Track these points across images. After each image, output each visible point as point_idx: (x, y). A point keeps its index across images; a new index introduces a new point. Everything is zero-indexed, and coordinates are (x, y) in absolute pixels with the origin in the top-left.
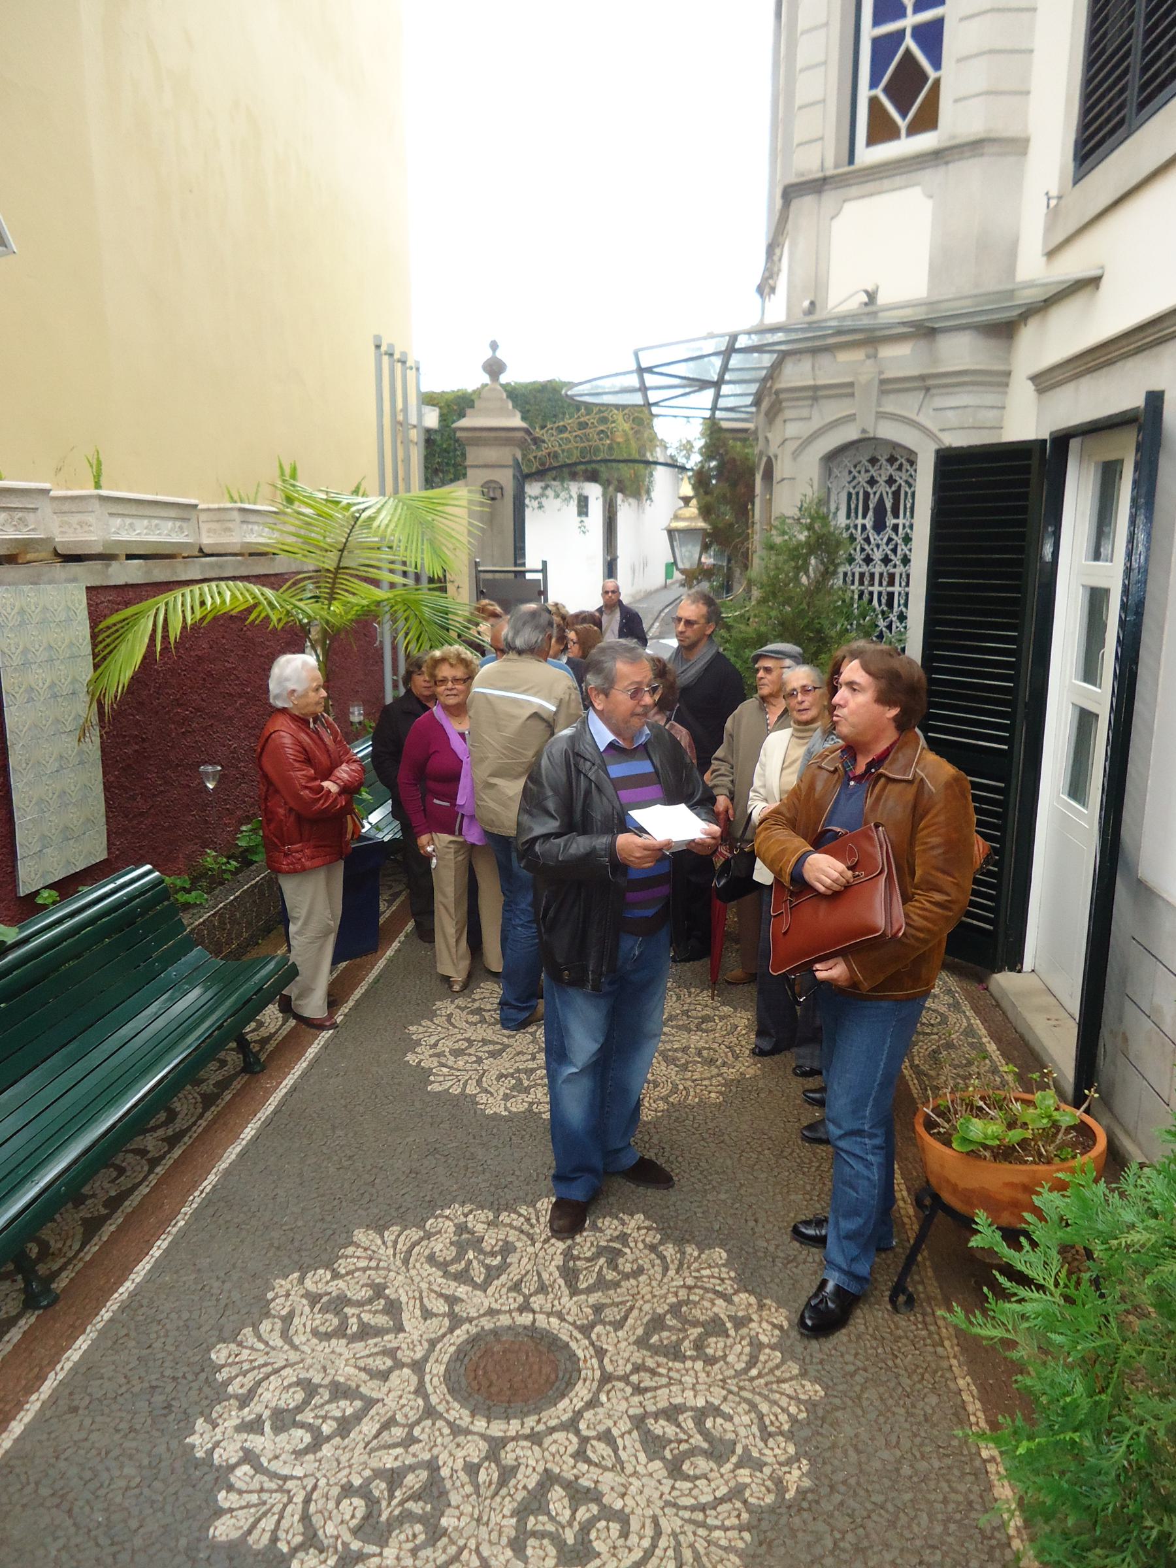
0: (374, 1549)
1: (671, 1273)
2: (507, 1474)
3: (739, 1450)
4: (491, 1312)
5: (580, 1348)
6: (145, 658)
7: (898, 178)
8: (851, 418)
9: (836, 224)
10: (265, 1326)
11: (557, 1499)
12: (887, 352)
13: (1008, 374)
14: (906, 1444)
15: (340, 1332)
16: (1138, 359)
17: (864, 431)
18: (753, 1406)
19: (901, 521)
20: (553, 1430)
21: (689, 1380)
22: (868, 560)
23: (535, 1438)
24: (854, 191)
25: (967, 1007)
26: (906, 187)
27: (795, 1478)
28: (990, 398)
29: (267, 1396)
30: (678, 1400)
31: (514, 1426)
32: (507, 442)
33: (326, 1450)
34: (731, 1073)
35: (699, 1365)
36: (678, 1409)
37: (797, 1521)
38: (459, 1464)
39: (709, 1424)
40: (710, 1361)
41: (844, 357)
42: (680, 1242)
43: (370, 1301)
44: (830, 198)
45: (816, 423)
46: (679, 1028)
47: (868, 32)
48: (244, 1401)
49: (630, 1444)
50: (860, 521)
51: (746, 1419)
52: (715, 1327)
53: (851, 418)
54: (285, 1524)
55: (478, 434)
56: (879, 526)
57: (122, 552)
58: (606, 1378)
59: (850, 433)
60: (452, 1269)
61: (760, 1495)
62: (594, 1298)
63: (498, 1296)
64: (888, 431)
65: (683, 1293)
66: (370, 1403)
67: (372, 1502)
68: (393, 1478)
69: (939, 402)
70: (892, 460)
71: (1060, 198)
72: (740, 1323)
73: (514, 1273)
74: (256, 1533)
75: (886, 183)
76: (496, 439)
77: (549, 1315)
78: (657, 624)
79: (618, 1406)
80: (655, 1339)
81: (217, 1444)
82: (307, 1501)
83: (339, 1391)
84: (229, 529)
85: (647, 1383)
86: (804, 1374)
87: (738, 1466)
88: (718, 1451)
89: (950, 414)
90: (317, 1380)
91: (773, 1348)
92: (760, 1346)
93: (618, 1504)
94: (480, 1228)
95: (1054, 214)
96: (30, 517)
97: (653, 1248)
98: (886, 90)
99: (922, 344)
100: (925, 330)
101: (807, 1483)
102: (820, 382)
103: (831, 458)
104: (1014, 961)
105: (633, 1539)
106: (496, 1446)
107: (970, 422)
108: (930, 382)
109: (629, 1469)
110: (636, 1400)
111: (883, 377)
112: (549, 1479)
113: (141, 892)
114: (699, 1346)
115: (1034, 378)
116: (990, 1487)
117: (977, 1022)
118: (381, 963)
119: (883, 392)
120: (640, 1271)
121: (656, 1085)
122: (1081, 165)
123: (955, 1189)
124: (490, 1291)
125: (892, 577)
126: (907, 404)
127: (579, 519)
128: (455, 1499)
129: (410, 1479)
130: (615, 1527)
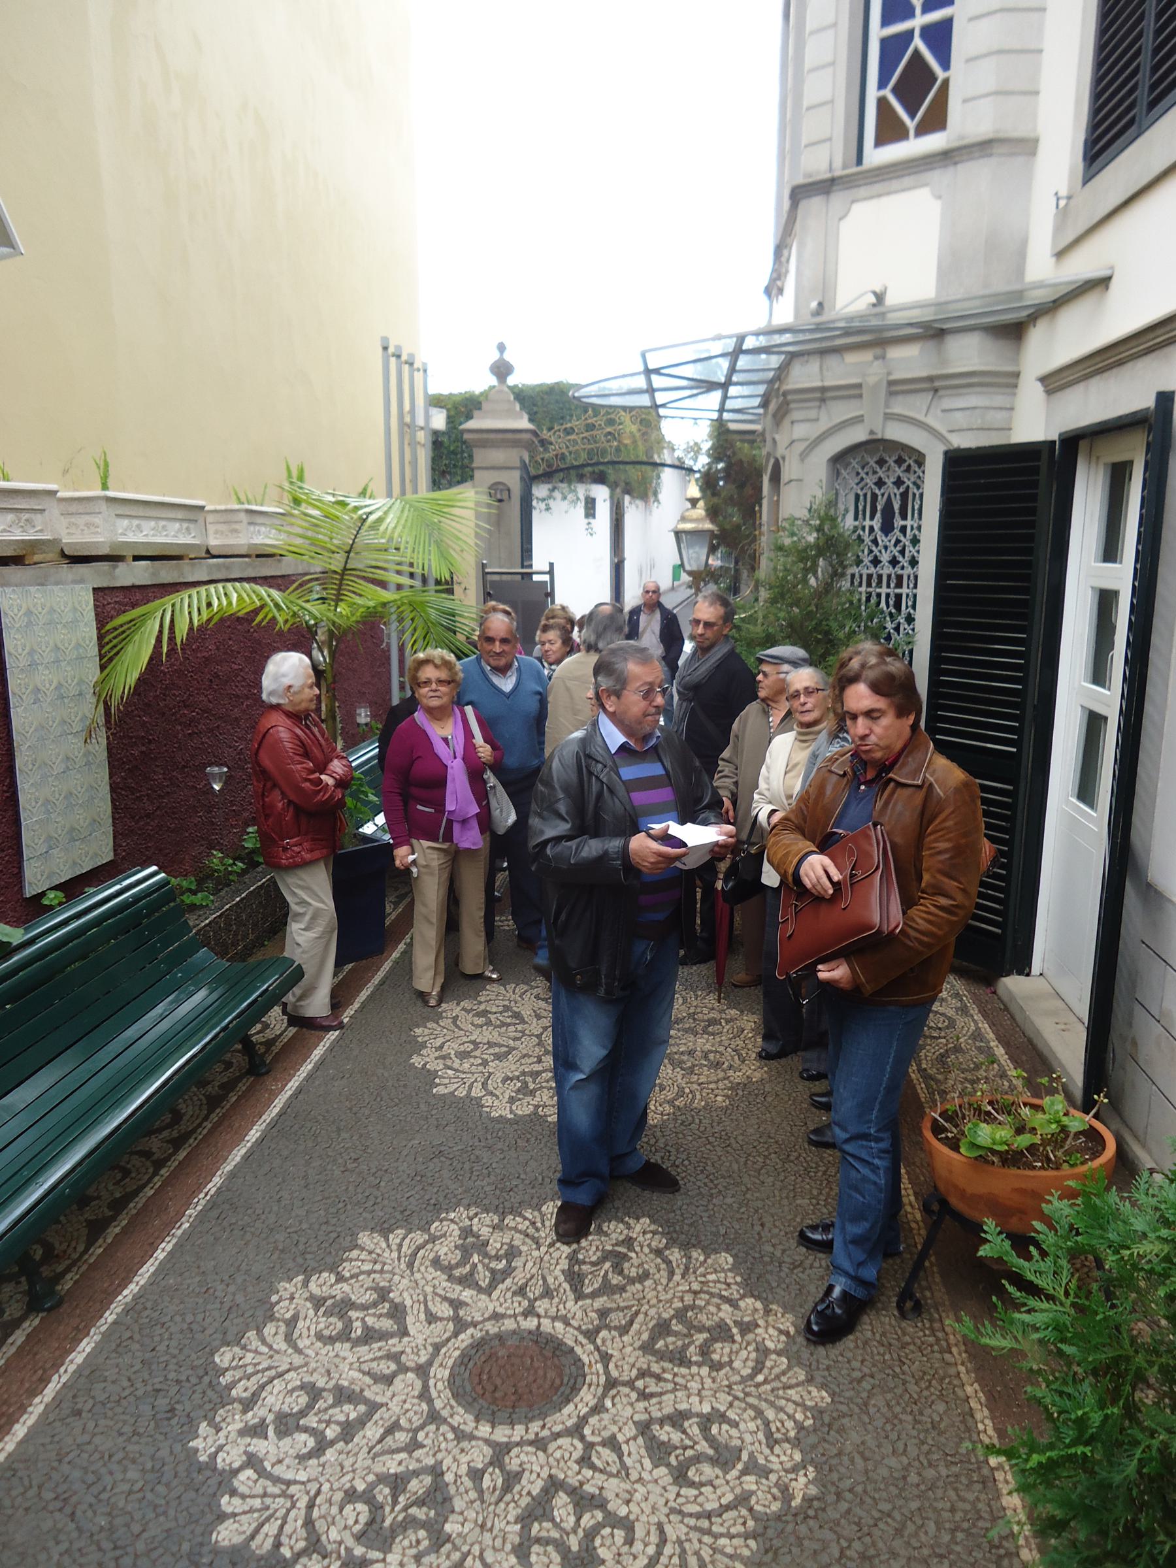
1: (677, 1278)
2: (512, 1479)
3: (745, 1456)
4: (496, 1316)
5: (585, 1353)
6: (151, 659)
8: (859, 420)
9: (843, 224)
10: (269, 1330)
11: (562, 1506)
12: (896, 353)
14: (913, 1451)
17: (872, 432)
18: (759, 1413)
19: (909, 523)
20: (558, 1435)
21: (694, 1385)
22: (876, 562)
23: (540, 1444)
24: (862, 191)
25: (974, 1010)
26: (914, 188)
27: (801, 1485)
28: (999, 400)
29: (270, 1400)
30: (683, 1406)
32: (516, 444)
33: (330, 1455)
34: (737, 1077)
35: (705, 1371)
36: (684, 1415)
37: (803, 1529)
38: (464, 1469)
39: (714, 1430)
40: (716, 1367)
41: (851, 358)
42: (686, 1247)
43: (375, 1305)
44: (838, 199)
45: (824, 424)
46: (686, 1031)
47: (877, 32)
48: (248, 1405)
49: (635, 1451)
50: (867, 523)
51: (752, 1426)
52: (721, 1332)
53: (859, 420)
54: (288, 1529)
55: (485, 436)
56: (887, 528)
58: (611, 1383)
59: (859, 435)
60: (457, 1273)
61: (766, 1503)
62: (600, 1302)
63: (502, 1301)
64: (896, 433)
65: (688, 1298)
66: (374, 1407)
67: (376, 1508)
68: (397, 1483)
70: (899, 461)
71: (1069, 198)
72: (747, 1328)
73: (519, 1277)
74: (259, 1538)
76: (503, 440)
79: (624, 1412)
80: (660, 1344)
81: (220, 1448)
82: (311, 1506)
83: (343, 1395)
84: (236, 531)
85: (653, 1388)
86: (810, 1380)
87: (744, 1472)
88: (724, 1457)
89: (958, 415)
90: (321, 1383)
91: (779, 1353)
92: (767, 1352)
93: (623, 1511)
94: (485, 1231)
95: (1063, 215)
97: (658, 1252)
98: (895, 91)
99: (930, 345)
100: (933, 332)
101: (813, 1491)
102: (827, 383)
103: (839, 460)
104: (1023, 965)
105: (638, 1546)
106: (500, 1451)
107: (979, 423)
108: (937, 384)
109: (634, 1476)
110: (641, 1405)
111: (892, 378)
112: (553, 1485)
114: (705, 1351)
115: (1043, 380)
117: (985, 1026)
119: (892, 394)
120: (646, 1275)
123: (962, 1194)
124: (495, 1295)
125: (900, 578)
126: (915, 406)
128: (458, 1504)
129: (414, 1485)
130: (620, 1534)
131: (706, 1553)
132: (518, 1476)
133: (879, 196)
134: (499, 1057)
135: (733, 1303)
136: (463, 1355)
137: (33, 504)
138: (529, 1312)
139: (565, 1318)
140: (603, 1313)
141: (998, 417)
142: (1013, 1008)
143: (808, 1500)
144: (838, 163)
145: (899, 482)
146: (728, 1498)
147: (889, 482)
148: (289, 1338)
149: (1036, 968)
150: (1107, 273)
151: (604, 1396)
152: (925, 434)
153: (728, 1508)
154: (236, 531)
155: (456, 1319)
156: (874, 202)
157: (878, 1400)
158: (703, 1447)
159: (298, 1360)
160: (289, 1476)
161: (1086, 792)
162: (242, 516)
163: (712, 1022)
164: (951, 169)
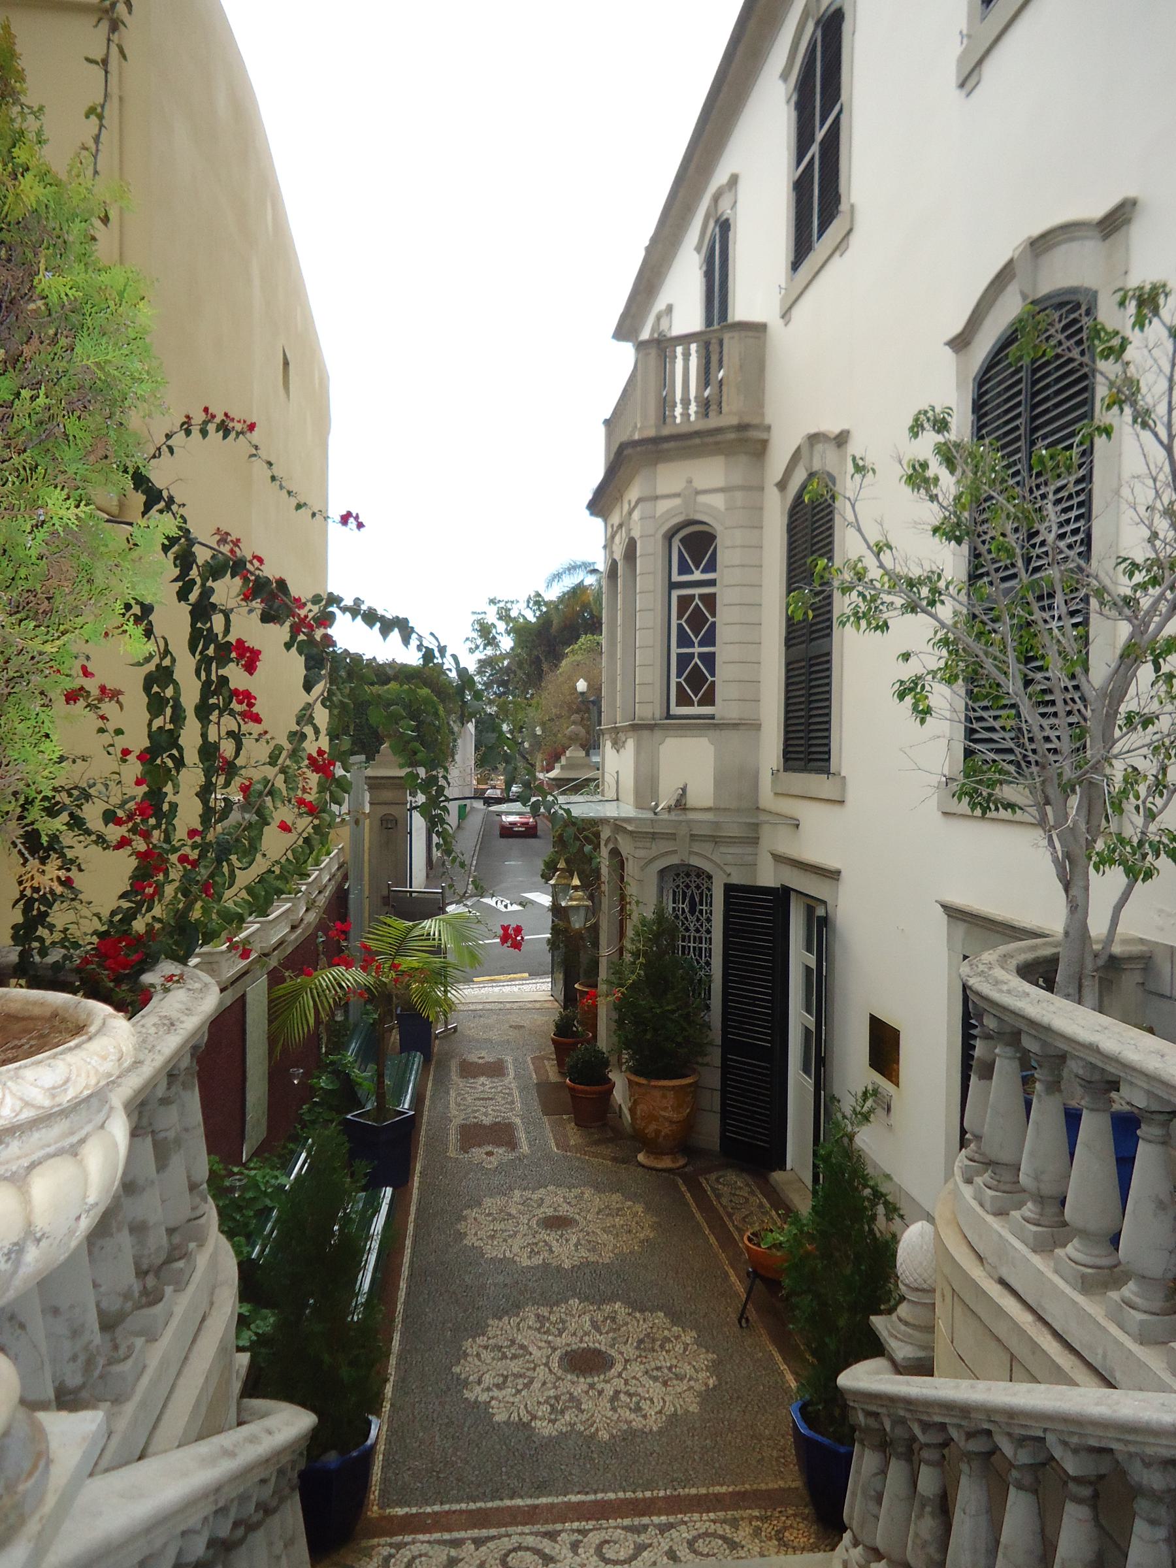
5: (612, 1352)
8: (675, 852)
19: (704, 908)
22: (687, 930)
25: (758, 1192)
27: (711, 1382)
28: (749, 850)
42: (642, 1311)
44: (658, 734)
45: (654, 852)
47: (675, 651)
52: (667, 1340)
53: (675, 852)
56: (692, 912)
58: (627, 1361)
59: (674, 860)
61: (698, 1387)
62: (611, 1335)
63: (565, 1338)
64: (695, 861)
68: (557, 1398)
69: (723, 849)
72: (678, 1337)
75: (688, 732)
98: (685, 680)
103: (662, 872)
104: (782, 1165)
112: (617, 1393)
125: (701, 938)
126: (706, 848)
135: (669, 1330)
138: (581, 1341)
139: (600, 1342)
143: (715, 1386)
144: (657, 715)
145: (698, 887)
147: (693, 885)
149: (788, 1167)
163: (619, 1209)
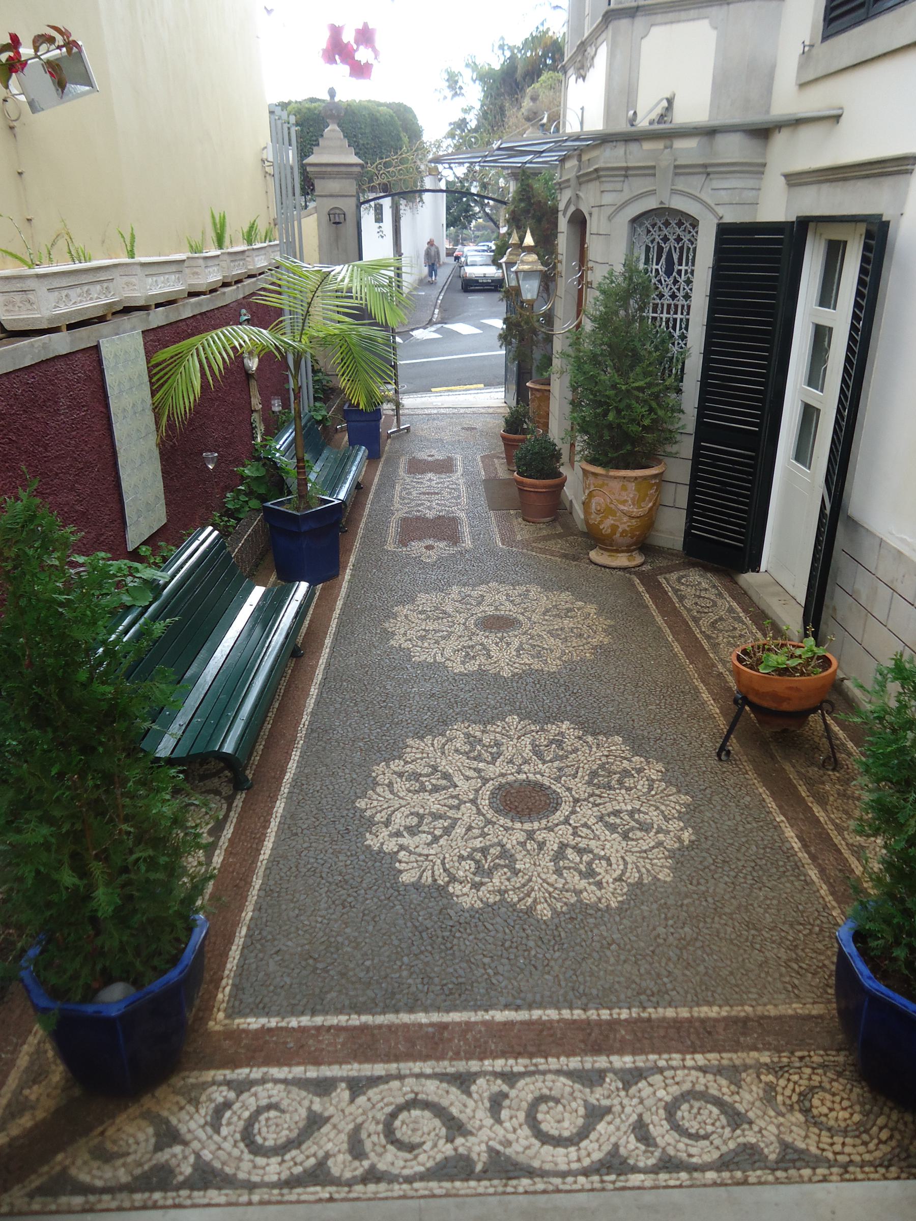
0: (487, 880)
1: (594, 749)
2: (541, 845)
3: (655, 826)
4: (503, 775)
5: (557, 787)
6: (202, 387)
7: (692, 12)
10: (379, 790)
11: (570, 853)
12: (681, 144)
13: (764, 165)
14: (738, 818)
15: (423, 789)
16: (867, 181)
17: (662, 203)
18: (657, 808)
19: (683, 268)
20: (557, 825)
21: (620, 798)
23: (550, 829)
24: (659, 18)
25: (726, 595)
26: (698, 19)
27: (686, 836)
28: (751, 183)
29: (398, 821)
30: (618, 808)
31: (536, 825)
32: (348, 175)
33: (442, 841)
34: (594, 642)
35: (623, 791)
36: (619, 812)
37: (693, 853)
38: (515, 842)
39: (636, 816)
40: (629, 789)
41: (647, 146)
42: (594, 734)
43: (433, 774)
44: (640, 22)
45: (626, 195)
46: (555, 616)
48: (387, 824)
49: (599, 828)
50: (655, 267)
51: (655, 813)
52: (626, 773)
53: (653, 192)
54: (437, 873)
55: (324, 169)
57: (153, 303)
59: (651, 203)
60: (472, 755)
61: (670, 843)
62: (556, 764)
65: (604, 759)
66: (455, 821)
67: (477, 862)
68: (484, 851)
69: (716, 184)
70: (680, 224)
71: (812, 46)
72: (640, 771)
73: (508, 755)
74: (424, 878)
76: (338, 173)
77: (535, 774)
78: (437, 311)
79: (587, 814)
80: (596, 781)
81: (382, 844)
82: (443, 864)
83: (436, 816)
84: (197, 273)
85: (599, 801)
86: (679, 792)
87: (657, 833)
88: (645, 827)
89: (723, 193)
90: (421, 811)
91: (660, 781)
92: (653, 781)
93: (602, 853)
94: (478, 734)
95: (807, 54)
96: (110, 285)
97: (580, 738)
99: (705, 140)
100: (710, 132)
101: (693, 838)
102: (630, 165)
104: (755, 565)
105: (614, 866)
106: (530, 835)
107: (737, 200)
108: (709, 170)
109: (603, 838)
110: (595, 809)
111: (677, 163)
112: (563, 846)
113: (210, 547)
114: (620, 782)
115: (787, 176)
116: (783, 833)
118: (345, 585)
119: (676, 174)
121: (552, 651)
122: (829, 25)
123: (757, 693)
124: (497, 764)
126: (693, 184)
127: (378, 225)
128: (519, 857)
129: (492, 851)
130: (604, 863)
131: (649, 866)
132: (544, 843)
133: (672, 22)
134: (443, 638)
136: (492, 793)
137: (103, 276)
139: (541, 772)
140: (560, 769)
141: (749, 195)
142: (750, 592)
146: (652, 844)
147: (672, 238)
148: (392, 792)
149: (763, 568)
150: (839, 112)
151: (574, 806)
152: (698, 205)
153: (653, 848)
154: (197, 273)
155: (482, 778)
156: (668, 27)
157: (716, 798)
158: (633, 823)
159: (403, 803)
160: (426, 852)
161: (802, 454)
162: (201, 262)
163: (569, 610)
164: (725, 7)
